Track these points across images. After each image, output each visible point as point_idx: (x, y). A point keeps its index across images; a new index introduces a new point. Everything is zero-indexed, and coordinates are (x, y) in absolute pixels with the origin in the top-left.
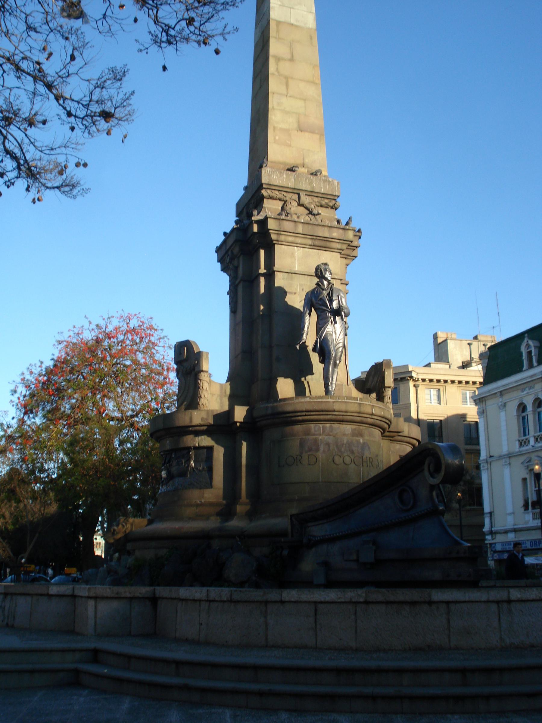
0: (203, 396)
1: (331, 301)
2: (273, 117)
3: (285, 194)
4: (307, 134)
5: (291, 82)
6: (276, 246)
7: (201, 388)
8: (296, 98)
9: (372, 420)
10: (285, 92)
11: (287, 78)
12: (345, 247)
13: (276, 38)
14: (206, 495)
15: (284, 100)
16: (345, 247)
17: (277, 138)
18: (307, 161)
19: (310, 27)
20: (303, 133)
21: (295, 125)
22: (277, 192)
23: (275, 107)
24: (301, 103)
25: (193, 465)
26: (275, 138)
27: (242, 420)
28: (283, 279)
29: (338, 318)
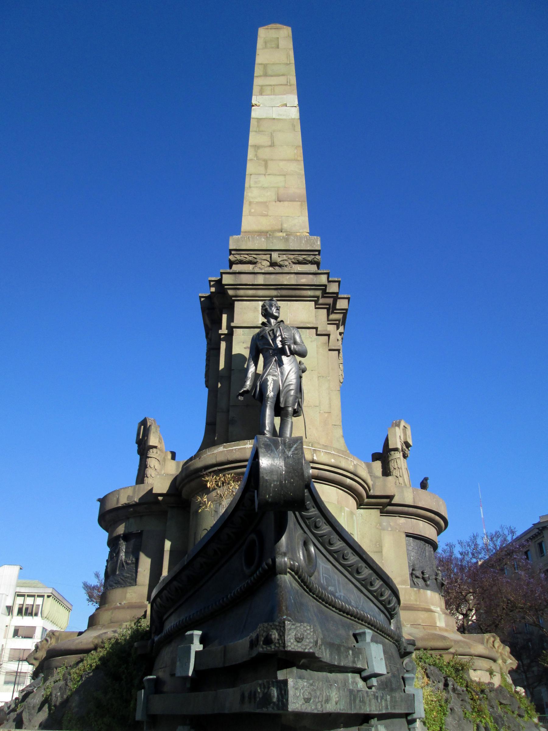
0: (149, 476)
1: (274, 339)
2: (250, 194)
3: (255, 256)
4: (286, 203)
5: (270, 164)
6: (236, 303)
7: (148, 466)
8: (276, 175)
9: (316, 471)
10: (263, 172)
11: (266, 162)
12: (319, 293)
13: (256, 132)
14: (128, 595)
15: (262, 179)
16: (319, 293)
17: (253, 211)
18: (285, 226)
19: (293, 117)
20: (282, 203)
21: (274, 197)
22: (246, 256)
23: (252, 185)
24: (281, 178)
25: (124, 557)
26: (250, 211)
27: (165, 491)
28: (243, 335)
29: (284, 358)
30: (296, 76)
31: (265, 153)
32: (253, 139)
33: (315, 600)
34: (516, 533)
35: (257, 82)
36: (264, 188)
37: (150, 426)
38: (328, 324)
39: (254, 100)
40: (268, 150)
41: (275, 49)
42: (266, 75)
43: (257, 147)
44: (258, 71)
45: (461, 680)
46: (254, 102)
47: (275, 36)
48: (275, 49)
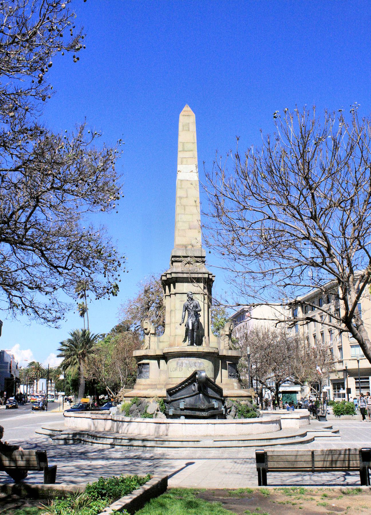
5: (186, 207)
30: (198, 151)
31: (184, 201)
32: (179, 193)
33: (326, 473)
34: (209, 377)
35: (180, 155)
36: (184, 222)
37: (185, 341)
38: (204, 257)
39: (179, 167)
40: (185, 199)
41: (187, 120)
42: (184, 150)
43: (181, 198)
44: (180, 148)
45: (106, 373)
46: (178, 169)
47: (188, 122)
48: (187, 120)
